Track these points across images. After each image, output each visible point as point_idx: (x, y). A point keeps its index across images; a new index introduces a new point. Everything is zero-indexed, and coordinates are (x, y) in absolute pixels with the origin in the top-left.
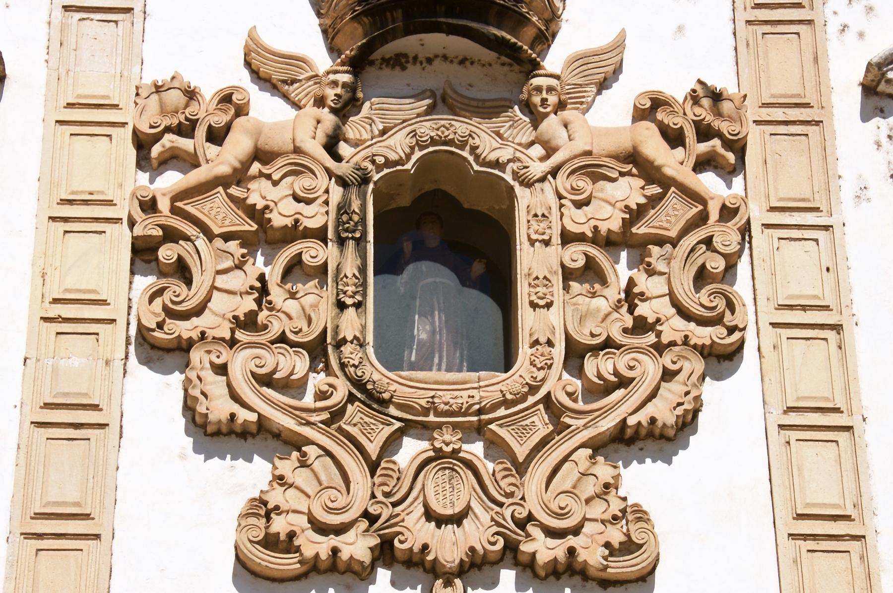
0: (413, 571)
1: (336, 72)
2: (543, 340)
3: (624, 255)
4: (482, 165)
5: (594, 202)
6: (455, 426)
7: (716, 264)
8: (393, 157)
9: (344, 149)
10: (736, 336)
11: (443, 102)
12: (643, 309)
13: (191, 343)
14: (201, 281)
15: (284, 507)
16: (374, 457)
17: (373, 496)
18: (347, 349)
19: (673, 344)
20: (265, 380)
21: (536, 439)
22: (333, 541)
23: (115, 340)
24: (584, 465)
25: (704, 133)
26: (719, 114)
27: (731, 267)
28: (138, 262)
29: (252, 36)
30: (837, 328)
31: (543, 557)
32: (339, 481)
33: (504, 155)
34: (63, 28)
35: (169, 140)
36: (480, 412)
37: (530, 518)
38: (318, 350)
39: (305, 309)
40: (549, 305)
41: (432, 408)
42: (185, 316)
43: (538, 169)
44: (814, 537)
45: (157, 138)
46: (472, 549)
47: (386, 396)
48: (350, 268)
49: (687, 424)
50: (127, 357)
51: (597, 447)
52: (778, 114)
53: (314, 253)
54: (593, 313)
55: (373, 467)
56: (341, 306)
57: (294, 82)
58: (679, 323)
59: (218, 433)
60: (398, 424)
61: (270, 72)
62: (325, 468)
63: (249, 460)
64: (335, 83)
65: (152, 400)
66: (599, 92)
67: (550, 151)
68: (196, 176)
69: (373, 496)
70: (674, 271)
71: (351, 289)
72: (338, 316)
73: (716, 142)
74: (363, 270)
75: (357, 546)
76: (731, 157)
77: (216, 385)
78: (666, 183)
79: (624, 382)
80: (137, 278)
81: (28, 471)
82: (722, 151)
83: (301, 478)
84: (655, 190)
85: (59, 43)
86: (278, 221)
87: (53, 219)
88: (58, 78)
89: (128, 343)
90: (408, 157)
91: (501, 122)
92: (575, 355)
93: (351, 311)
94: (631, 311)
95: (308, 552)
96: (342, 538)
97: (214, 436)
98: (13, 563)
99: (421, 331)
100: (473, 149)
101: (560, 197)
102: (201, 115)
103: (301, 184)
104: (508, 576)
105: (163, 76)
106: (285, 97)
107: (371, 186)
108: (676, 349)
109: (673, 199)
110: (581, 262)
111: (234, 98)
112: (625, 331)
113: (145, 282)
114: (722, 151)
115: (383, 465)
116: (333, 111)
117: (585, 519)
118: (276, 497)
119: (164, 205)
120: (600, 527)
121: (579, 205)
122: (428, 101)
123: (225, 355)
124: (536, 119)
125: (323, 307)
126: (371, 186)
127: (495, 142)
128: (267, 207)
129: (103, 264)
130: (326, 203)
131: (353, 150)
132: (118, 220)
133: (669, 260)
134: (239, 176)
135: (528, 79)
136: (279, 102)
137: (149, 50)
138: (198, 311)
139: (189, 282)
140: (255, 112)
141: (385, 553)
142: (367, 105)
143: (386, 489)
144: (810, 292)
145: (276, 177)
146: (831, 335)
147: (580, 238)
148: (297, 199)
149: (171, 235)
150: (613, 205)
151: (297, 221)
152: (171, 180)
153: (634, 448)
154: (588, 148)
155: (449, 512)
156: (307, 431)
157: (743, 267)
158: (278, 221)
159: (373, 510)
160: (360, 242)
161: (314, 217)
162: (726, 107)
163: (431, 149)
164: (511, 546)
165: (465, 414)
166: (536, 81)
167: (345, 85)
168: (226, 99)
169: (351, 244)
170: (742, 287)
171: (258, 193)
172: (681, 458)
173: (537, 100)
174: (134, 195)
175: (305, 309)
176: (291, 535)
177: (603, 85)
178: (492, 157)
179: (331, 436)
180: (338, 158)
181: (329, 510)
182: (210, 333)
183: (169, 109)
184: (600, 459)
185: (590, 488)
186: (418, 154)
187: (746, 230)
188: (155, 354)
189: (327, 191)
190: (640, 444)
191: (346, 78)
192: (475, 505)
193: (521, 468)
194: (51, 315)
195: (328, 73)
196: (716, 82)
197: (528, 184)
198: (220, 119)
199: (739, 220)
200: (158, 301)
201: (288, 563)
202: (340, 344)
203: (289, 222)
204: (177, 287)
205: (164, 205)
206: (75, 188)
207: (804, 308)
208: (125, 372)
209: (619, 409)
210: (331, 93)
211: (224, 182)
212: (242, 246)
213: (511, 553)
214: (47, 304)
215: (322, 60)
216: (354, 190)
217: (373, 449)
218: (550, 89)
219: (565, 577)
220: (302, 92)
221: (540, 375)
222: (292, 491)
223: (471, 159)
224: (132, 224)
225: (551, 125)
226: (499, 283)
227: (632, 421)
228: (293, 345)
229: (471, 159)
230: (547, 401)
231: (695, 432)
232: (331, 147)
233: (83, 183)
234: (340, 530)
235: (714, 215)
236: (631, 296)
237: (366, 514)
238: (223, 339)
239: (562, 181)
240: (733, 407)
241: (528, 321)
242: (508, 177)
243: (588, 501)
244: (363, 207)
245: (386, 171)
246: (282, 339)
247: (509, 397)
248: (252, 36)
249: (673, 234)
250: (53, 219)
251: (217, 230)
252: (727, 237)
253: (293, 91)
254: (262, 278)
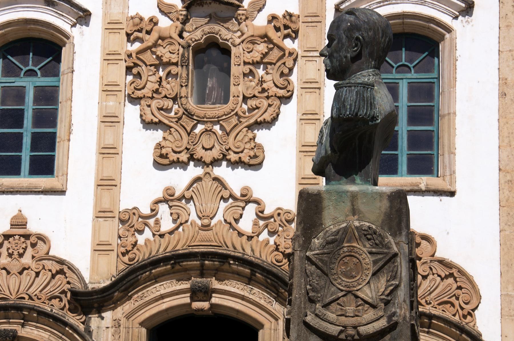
0: (200, 162)
1: (182, 11)
2: (236, 96)
3: (262, 66)
4: (223, 40)
5: (254, 51)
6: (211, 122)
7: (286, 71)
8: (197, 39)
9: (185, 35)
10: (290, 93)
11: (213, 18)
12: (265, 86)
13: (141, 98)
14: (144, 78)
15: (165, 146)
16: (189, 132)
17: (188, 143)
18: (183, 99)
19: (272, 96)
21: (232, 126)
22: (178, 155)
24: (245, 133)
25: (286, 27)
26: (292, 21)
27: (291, 70)
28: (128, 72)
30: (319, 88)
32: (180, 138)
33: (228, 37)
35: (136, 34)
36: (218, 117)
37: (230, 149)
39: (171, 87)
40: (238, 85)
42: (140, 90)
44: (306, 152)
45: (132, 34)
46: (214, 158)
47: (193, 113)
48: (184, 75)
49: (275, 119)
50: (125, 101)
51: (250, 127)
52: (309, 19)
53: (174, 70)
54: (250, 86)
55: (189, 134)
57: (171, 13)
58: (275, 89)
60: (196, 122)
62: (176, 135)
63: (157, 131)
64: (181, 15)
65: (132, 113)
66: (258, 13)
67: (243, 34)
69: (188, 143)
71: (184, 81)
72: (181, 89)
73: (290, 30)
74: (188, 75)
75: (184, 157)
76: (294, 35)
77: (148, 110)
79: (258, 108)
80: (128, 76)
82: (291, 33)
84: (271, 46)
86: (165, 60)
87: (105, 60)
88: (105, 15)
89: (125, 96)
90: (202, 38)
91: (228, 25)
92: (245, 99)
93: (184, 88)
94: (261, 86)
95: (171, 159)
96: (180, 154)
98: (98, 161)
100: (220, 35)
101: (244, 50)
102: (144, 27)
103: (172, 48)
106: (169, 17)
107: (191, 48)
108: (272, 98)
110: (248, 71)
111: (153, 20)
112: (259, 92)
113: (130, 78)
114: (291, 33)
115: (192, 133)
116: (181, 23)
117: (244, 148)
118: (163, 144)
119: (134, 55)
120: (248, 151)
121: (249, 52)
122: (208, 19)
123: (149, 102)
125: (176, 87)
126: (191, 48)
127: (225, 33)
128: (162, 56)
130: (178, 54)
131: (188, 34)
132: (122, 60)
133: (273, 69)
135: (237, 11)
136: (167, 18)
138: (143, 88)
139: (141, 78)
141: (191, 158)
142: (191, 20)
143: (192, 141)
144: (313, 77)
145: (164, 46)
146: (317, 90)
147: (249, 63)
148: (171, 53)
149: (136, 65)
150: (258, 52)
151: (170, 60)
152: (137, 46)
153: (261, 126)
154: (252, 34)
155: (208, 147)
156: (172, 124)
157: (295, 70)
158: (165, 60)
159: (188, 147)
160: (187, 66)
161: (174, 58)
163: (208, 35)
165: (214, 118)
166: (239, 12)
167: (184, 15)
168: (151, 20)
169: (184, 67)
170: (294, 78)
171: (160, 51)
172: (273, 128)
173: (239, 18)
174: (125, 53)
175: (171, 87)
176: (167, 154)
177: (260, 10)
178: (225, 38)
179: (178, 126)
181: (177, 147)
182: (146, 96)
183: (136, 24)
184: (250, 131)
185: (246, 139)
186: (205, 37)
188: (132, 100)
189: (178, 50)
190: (262, 125)
191: (184, 13)
192: (216, 144)
193: (228, 134)
194: (105, 89)
195: (180, 11)
196: (291, 11)
197: (235, 46)
198: (149, 28)
200: (133, 85)
202: (181, 98)
203: (168, 60)
205: (134, 55)
206: (110, 50)
207: (311, 82)
208: (125, 105)
209: (257, 116)
210: (181, 17)
212: (155, 68)
214: (104, 86)
216: (186, 50)
217: (189, 129)
218: (243, 15)
219: (239, 164)
221: (235, 106)
222: (167, 141)
223: (219, 38)
224: (126, 61)
227: (259, 120)
228: (168, 98)
229: (219, 38)
230: (236, 114)
231: (277, 121)
232: (181, 36)
234: (180, 152)
235: (287, 55)
236: (262, 82)
237: (186, 148)
238: (149, 97)
241: (233, 89)
242: (229, 44)
243: (246, 143)
244: (188, 55)
245: (195, 42)
246: (166, 96)
247: (226, 113)
249: (274, 62)
250: (105, 60)
251: (148, 63)
252: (289, 63)
254: (161, 78)
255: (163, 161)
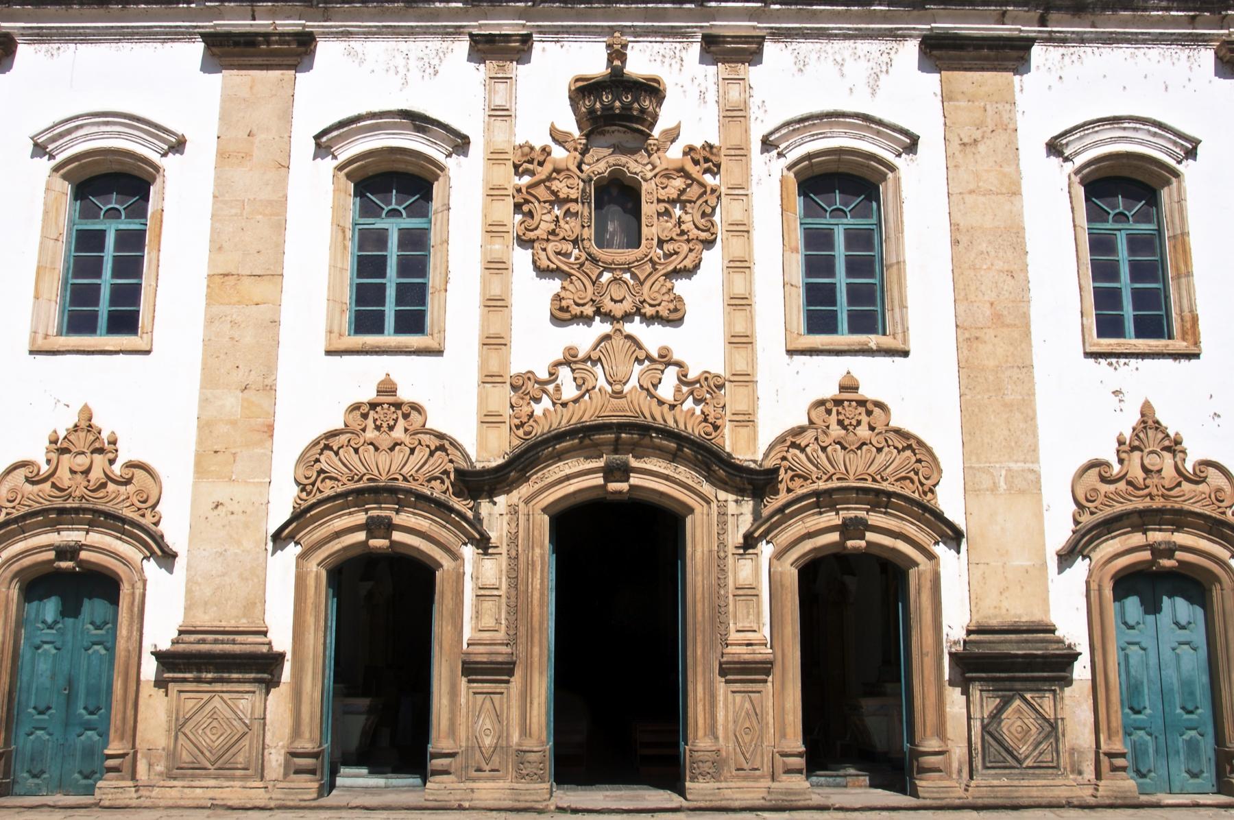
7: (709, 210)
9: (585, 167)
11: (618, 149)
12: (684, 227)
20: (558, 253)
22: (581, 308)
23: (510, 238)
25: (707, 160)
26: (712, 153)
27: (714, 209)
29: (552, 125)
31: (648, 314)
34: (489, 124)
35: (526, 165)
38: (575, 242)
39: (570, 227)
41: (613, 263)
43: (650, 175)
48: (586, 213)
49: (697, 267)
51: (668, 276)
52: (733, 152)
53: (574, 207)
54: (666, 228)
55: (594, 283)
56: (583, 227)
58: (695, 231)
59: (544, 271)
61: (558, 137)
65: (522, 259)
67: (654, 167)
68: (536, 178)
70: (694, 212)
75: (589, 310)
77: (543, 255)
78: (693, 180)
79: (676, 253)
81: (485, 284)
83: (571, 287)
85: (488, 129)
86: (562, 196)
88: (488, 143)
91: (637, 157)
92: (661, 243)
97: (543, 272)
99: (610, 228)
103: (570, 181)
104: (637, 319)
105: (522, 142)
109: (695, 186)
113: (519, 217)
118: (563, 294)
119: (524, 190)
123: (544, 245)
124: (650, 155)
127: (635, 165)
129: (504, 211)
134: (549, 178)
137: (517, 130)
138: (536, 228)
139: (532, 217)
140: (553, 155)
141: (598, 312)
147: (663, 201)
149: (527, 201)
152: (526, 179)
157: (718, 210)
158: (562, 196)
160: (589, 203)
161: (574, 194)
162: (715, 150)
164: (638, 310)
168: (543, 149)
171: (555, 185)
172: (695, 278)
175: (570, 227)
177: (673, 141)
180: (582, 171)
185: (664, 290)
187: (719, 197)
191: (584, 141)
193: (642, 284)
197: (646, 180)
198: (541, 158)
199: (717, 194)
201: (567, 316)
202: (583, 240)
204: (529, 220)
205: (524, 190)
209: (675, 263)
210: (579, 147)
211: (543, 181)
213: (638, 311)
215: (576, 133)
220: (570, 145)
225: (655, 157)
226: (636, 212)
233: (497, 182)
234: (583, 305)
236: (680, 222)
239: (658, 180)
240: (712, 260)
241: (645, 231)
246: (564, 239)
248: (552, 125)
252: (712, 200)
253: (567, 145)
255: (562, 316)
